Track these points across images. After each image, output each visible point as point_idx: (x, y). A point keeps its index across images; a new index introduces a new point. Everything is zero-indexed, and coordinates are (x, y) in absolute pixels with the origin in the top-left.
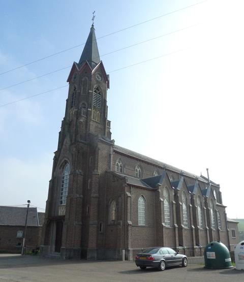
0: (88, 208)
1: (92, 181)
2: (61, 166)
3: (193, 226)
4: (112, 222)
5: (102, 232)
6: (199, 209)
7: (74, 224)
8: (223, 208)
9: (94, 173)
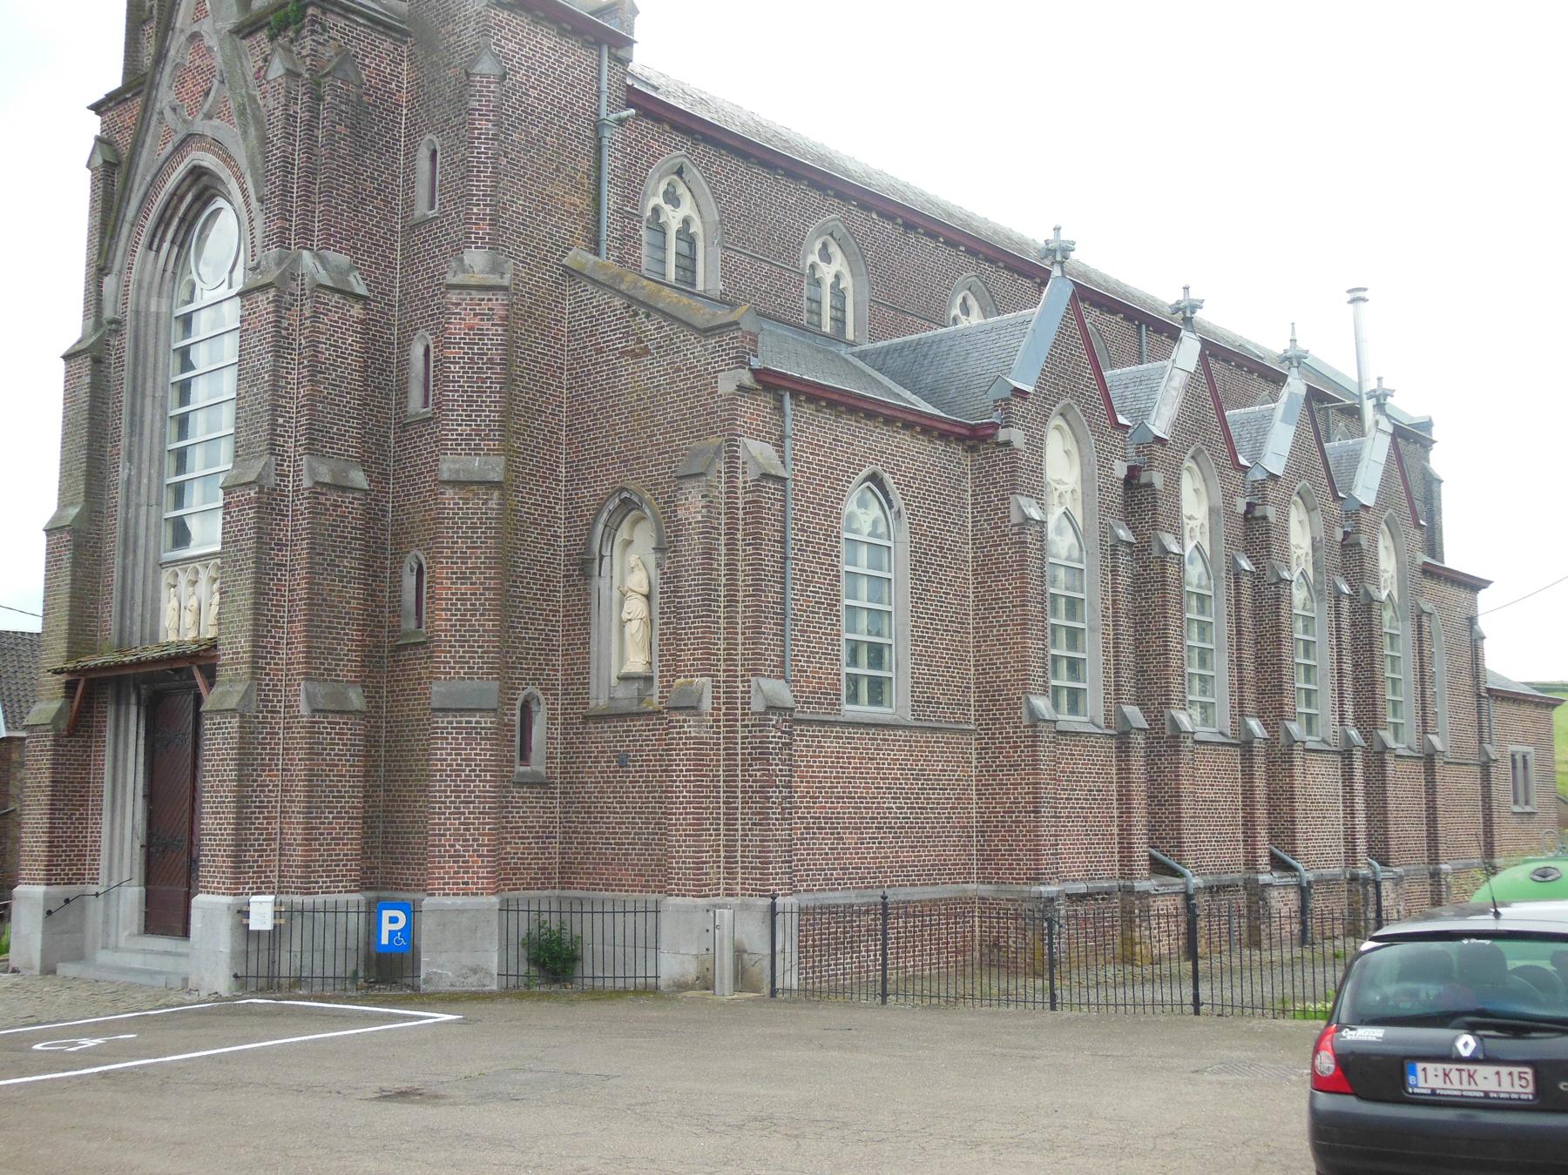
0: (409, 581)
1: (443, 345)
2: (163, 221)
3: (1254, 724)
4: (625, 693)
5: (538, 765)
6: (152, 538)
7: (304, 708)
8: (1463, 594)
9: (451, 279)
